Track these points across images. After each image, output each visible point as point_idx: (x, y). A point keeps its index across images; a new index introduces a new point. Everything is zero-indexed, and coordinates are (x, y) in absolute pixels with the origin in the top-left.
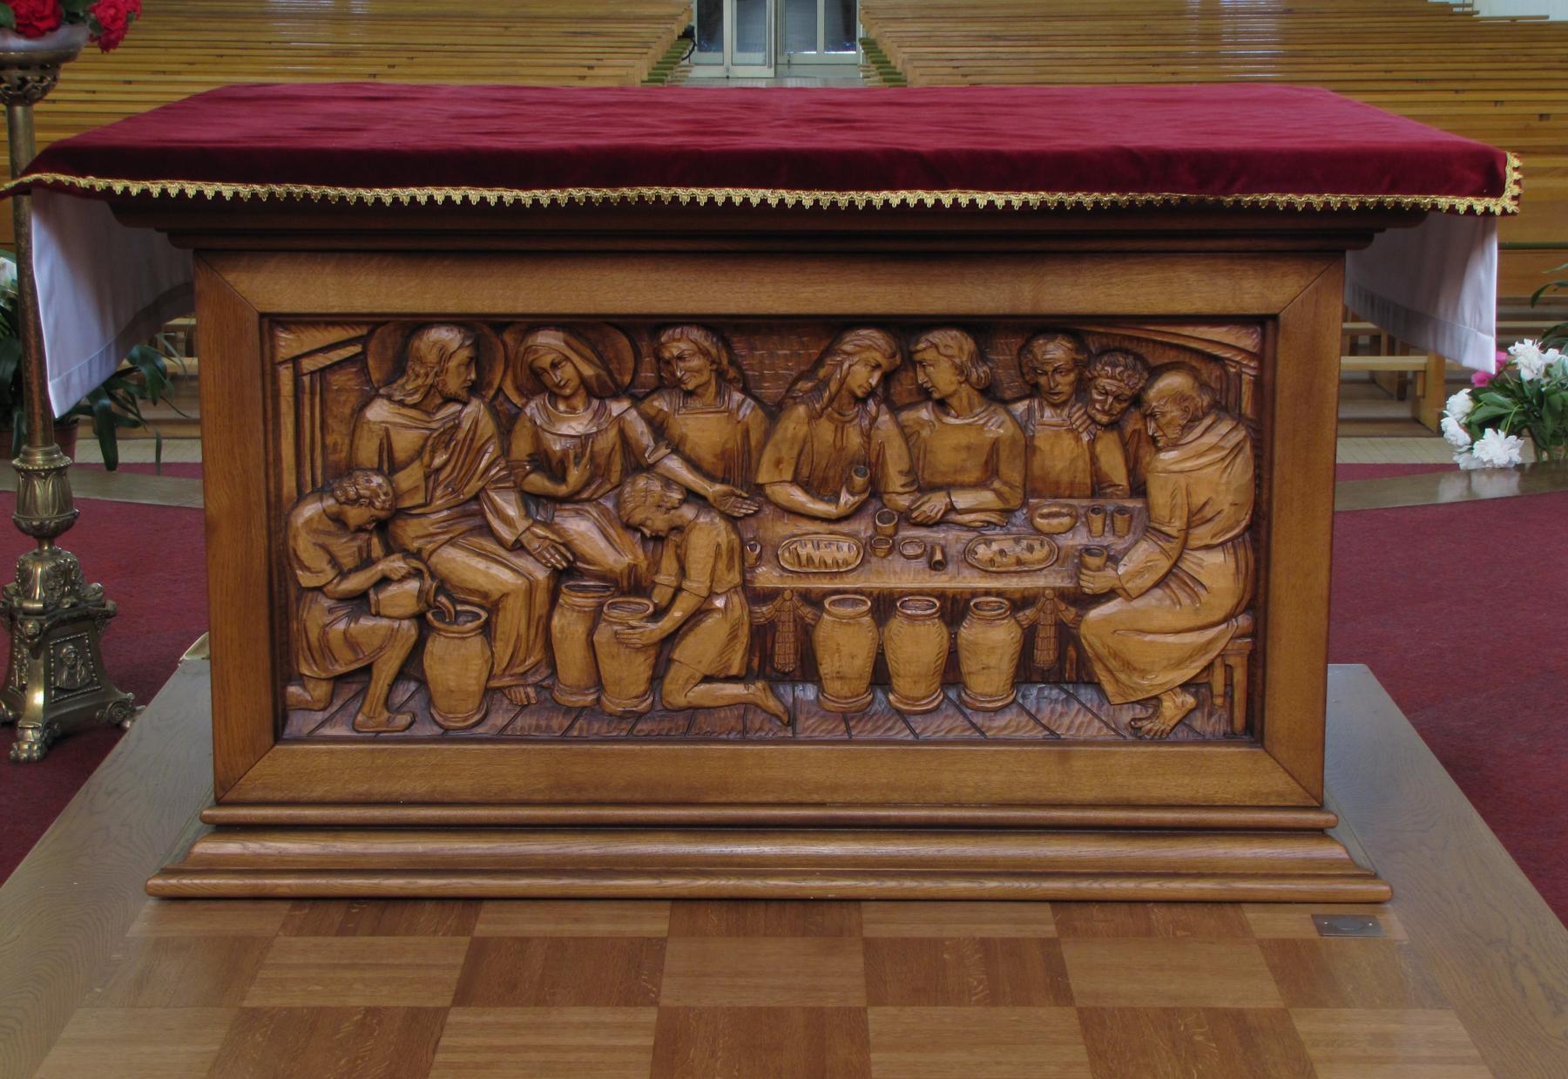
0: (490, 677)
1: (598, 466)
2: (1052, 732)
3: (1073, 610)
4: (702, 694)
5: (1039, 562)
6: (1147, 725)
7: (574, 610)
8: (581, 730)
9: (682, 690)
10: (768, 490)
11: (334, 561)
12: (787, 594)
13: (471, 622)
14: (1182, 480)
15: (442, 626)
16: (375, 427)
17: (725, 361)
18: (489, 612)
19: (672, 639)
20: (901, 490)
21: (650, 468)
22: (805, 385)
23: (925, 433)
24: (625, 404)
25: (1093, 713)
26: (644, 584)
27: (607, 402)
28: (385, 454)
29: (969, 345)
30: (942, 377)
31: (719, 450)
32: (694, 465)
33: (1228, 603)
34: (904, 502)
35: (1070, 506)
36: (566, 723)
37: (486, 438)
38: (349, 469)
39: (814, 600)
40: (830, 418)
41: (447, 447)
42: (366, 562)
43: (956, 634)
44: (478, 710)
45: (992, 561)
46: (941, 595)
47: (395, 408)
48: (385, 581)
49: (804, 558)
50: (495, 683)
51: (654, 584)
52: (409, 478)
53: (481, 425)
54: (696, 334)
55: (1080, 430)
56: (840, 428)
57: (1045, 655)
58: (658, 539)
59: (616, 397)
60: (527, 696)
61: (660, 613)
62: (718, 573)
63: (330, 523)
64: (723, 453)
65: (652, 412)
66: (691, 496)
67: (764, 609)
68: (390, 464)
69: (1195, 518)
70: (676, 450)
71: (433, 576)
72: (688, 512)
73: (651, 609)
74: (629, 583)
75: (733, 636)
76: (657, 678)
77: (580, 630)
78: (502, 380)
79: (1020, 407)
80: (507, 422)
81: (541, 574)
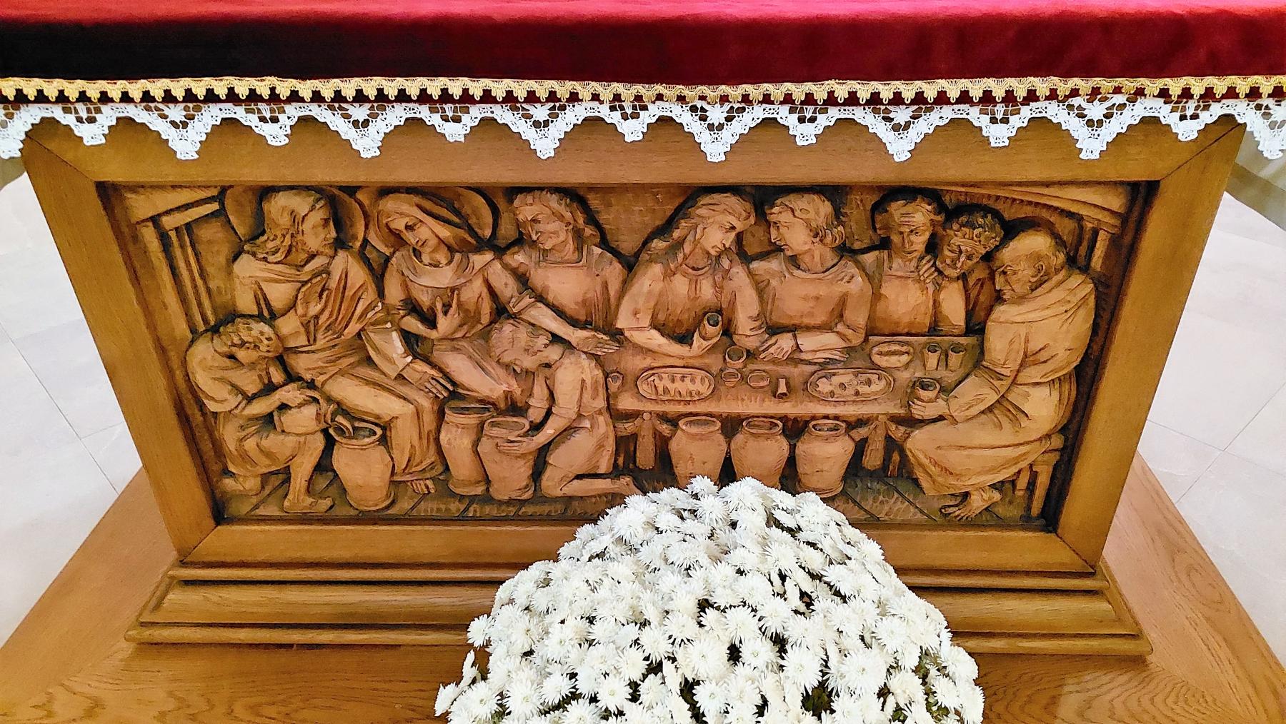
0: (393, 473)
1: (467, 311)
2: (872, 515)
3: (902, 429)
4: (578, 488)
5: (876, 393)
6: (956, 512)
7: (458, 427)
8: (475, 511)
9: (552, 483)
10: (627, 334)
11: (236, 389)
12: (646, 416)
13: (369, 437)
14: (1023, 330)
15: (344, 441)
16: (247, 281)
17: (581, 221)
18: (384, 428)
19: (544, 451)
20: (749, 333)
21: (515, 317)
22: (658, 244)
23: (774, 283)
24: (489, 256)
25: (909, 502)
26: (519, 405)
27: (470, 255)
28: (262, 302)
29: (825, 208)
30: (796, 237)
31: (580, 300)
32: (559, 312)
33: (1046, 427)
34: (752, 343)
35: (907, 343)
36: (462, 507)
37: (358, 286)
38: (231, 316)
39: (673, 421)
40: (685, 274)
41: (320, 296)
42: (270, 388)
43: (795, 445)
44: (388, 496)
45: (832, 394)
46: (784, 419)
47: (262, 264)
48: (283, 407)
49: (660, 389)
50: (396, 478)
51: (529, 406)
52: (289, 325)
53: (351, 275)
54: (553, 200)
55: (928, 281)
56: (694, 282)
57: (873, 459)
58: (529, 374)
59: (478, 250)
60: (427, 487)
61: (537, 427)
62: (584, 400)
63: (225, 359)
64: (584, 302)
65: (514, 265)
66: (556, 339)
67: (626, 425)
68: (268, 314)
69: (1028, 359)
70: (541, 298)
71: (329, 400)
72: (554, 353)
73: (527, 427)
74: (506, 404)
75: (600, 446)
76: (537, 474)
77: (466, 442)
78: (365, 232)
79: (869, 258)
80: (378, 275)
81: (426, 403)
